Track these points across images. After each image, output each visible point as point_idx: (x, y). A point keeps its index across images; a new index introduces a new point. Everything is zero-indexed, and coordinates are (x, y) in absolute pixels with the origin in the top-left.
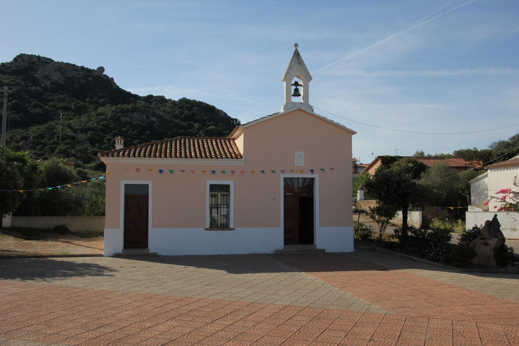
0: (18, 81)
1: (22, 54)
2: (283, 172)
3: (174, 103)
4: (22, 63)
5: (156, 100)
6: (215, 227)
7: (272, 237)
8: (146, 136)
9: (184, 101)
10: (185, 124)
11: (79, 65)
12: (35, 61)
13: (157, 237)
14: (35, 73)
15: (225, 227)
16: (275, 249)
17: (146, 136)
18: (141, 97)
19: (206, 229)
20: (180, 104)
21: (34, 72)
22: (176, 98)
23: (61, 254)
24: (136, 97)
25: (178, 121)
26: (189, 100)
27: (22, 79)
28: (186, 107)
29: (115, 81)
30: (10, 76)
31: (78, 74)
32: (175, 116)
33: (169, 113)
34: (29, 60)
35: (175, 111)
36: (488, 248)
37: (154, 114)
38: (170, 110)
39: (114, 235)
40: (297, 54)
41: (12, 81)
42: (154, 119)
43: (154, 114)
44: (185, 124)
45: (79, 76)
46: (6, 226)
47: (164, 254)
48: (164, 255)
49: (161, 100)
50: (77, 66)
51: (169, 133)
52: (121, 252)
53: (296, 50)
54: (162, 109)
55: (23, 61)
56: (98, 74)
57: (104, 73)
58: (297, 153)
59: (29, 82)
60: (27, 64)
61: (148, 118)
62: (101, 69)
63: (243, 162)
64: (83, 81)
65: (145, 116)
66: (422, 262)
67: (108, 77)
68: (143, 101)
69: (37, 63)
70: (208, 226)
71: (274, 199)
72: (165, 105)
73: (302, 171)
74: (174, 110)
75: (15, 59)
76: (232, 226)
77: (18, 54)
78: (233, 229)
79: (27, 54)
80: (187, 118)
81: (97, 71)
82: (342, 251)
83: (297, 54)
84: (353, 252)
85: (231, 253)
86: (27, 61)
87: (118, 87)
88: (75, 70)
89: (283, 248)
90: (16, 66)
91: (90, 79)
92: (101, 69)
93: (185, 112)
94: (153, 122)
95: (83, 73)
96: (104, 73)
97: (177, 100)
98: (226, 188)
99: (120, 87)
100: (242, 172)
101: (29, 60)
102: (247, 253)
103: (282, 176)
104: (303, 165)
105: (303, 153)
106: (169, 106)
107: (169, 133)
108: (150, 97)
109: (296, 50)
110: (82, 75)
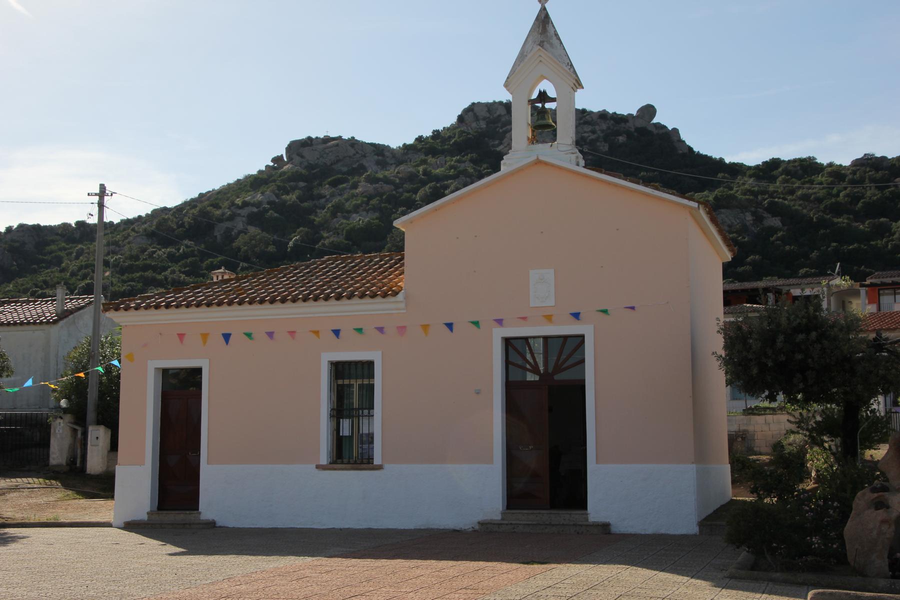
0: (462, 166)
1: (473, 104)
2: (500, 322)
3: (836, 173)
4: (474, 125)
5: (787, 172)
6: (349, 463)
7: (478, 486)
8: (748, 268)
9: (870, 165)
10: (863, 227)
11: (595, 110)
12: (500, 116)
13: (220, 488)
14: (501, 144)
15: (365, 461)
16: (481, 517)
17: (748, 268)
18: (750, 168)
19: (319, 467)
20: (854, 173)
21: (497, 142)
22: (843, 156)
23: (53, 521)
24: (736, 169)
25: (842, 221)
26: (884, 158)
27: (472, 161)
28: (872, 180)
29: (683, 137)
30: (448, 158)
31: (593, 132)
32: (837, 209)
33: (819, 200)
34: (488, 115)
35: (838, 195)
36: (881, 514)
37: (773, 209)
38: (821, 194)
39: (137, 481)
40: (543, 21)
41: (451, 167)
42: (776, 222)
43: (773, 209)
44: (863, 227)
45: (593, 137)
46: (92, 473)
47: (231, 523)
48: (231, 526)
49: (806, 168)
50: (591, 112)
51: (814, 255)
52: (145, 517)
53: (544, 9)
54: (799, 193)
55: (477, 118)
56: (639, 124)
57: (655, 120)
58: (534, 275)
59: (485, 166)
60: (483, 125)
61: (758, 219)
62: (649, 111)
63: (403, 305)
64: (605, 147)
65: (749, 218)
66: (16, 489)
67: (665, 127)
68: (750, 176)
69: (503, 119)
70: (324, 460)
71: (478, 393)
72: (811, 182)
73: (549, 318)
74: (835, 191)
75: (461, 118)
76: (377, 461)
77: (466, 106)
78: (380, 467)
79: (483, 101)
80: (874, 210)
81: (637, 116)
82: (663, 531)
83: (543, 21)
84: (695, 535)
85: (374, 525)
86: (484, 119)
87: (690, 149)
88: (586, 123)
89: (499, 517)
90: (462, 132)
91: (622, 139)
92: (649, 111)
93: (869, 193)
94: (773, 230)
95: (604, 126)
96: (655, 120)
97: (846, 162)
98: (367, 367)
99: (696, 150)
100: (402, 329)
101: (488, 115)
102: (411, 526)
103: (499, 334)
104: (551, 302)
105: (552, 271)
106: (821, 183)
107: (814, 255)
108: (774, 164)
109: (544, 9)
110: (602, 131)
